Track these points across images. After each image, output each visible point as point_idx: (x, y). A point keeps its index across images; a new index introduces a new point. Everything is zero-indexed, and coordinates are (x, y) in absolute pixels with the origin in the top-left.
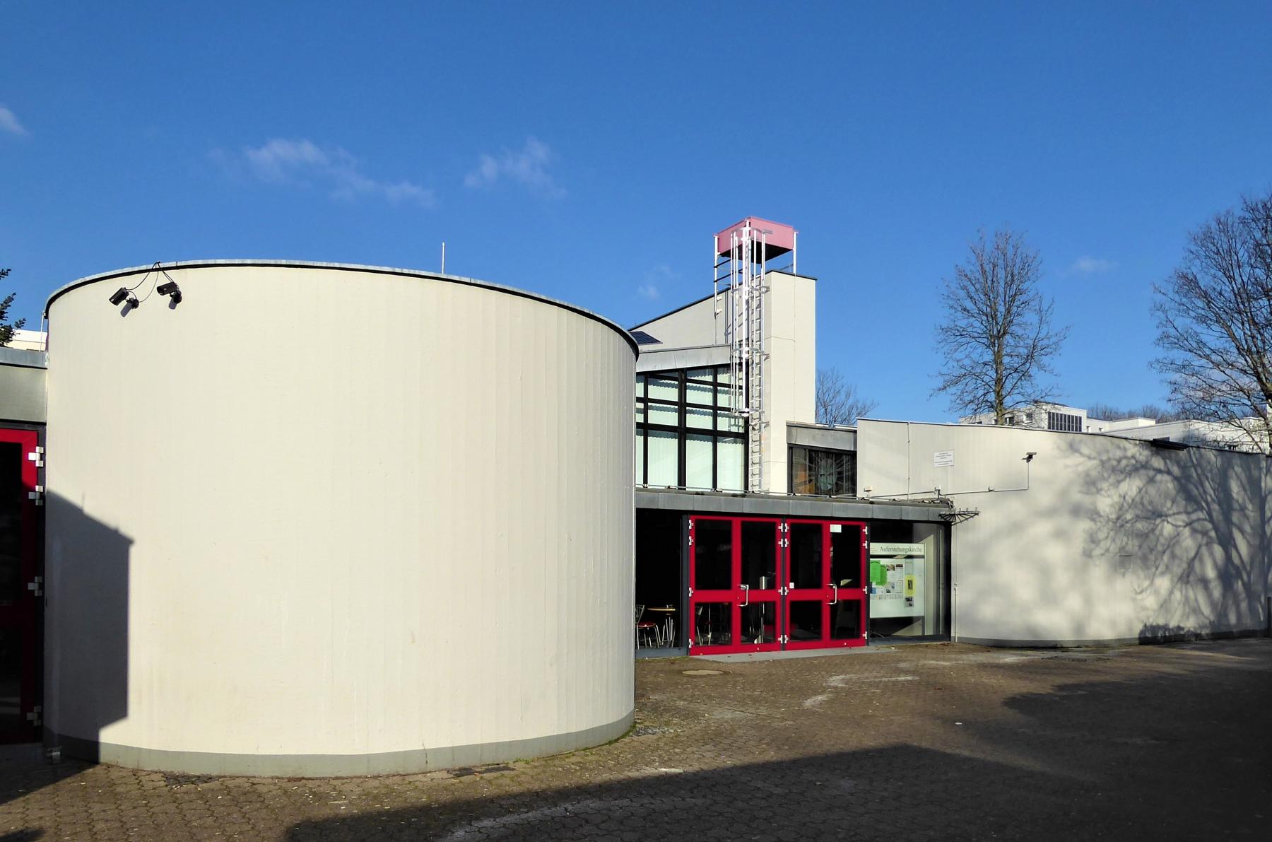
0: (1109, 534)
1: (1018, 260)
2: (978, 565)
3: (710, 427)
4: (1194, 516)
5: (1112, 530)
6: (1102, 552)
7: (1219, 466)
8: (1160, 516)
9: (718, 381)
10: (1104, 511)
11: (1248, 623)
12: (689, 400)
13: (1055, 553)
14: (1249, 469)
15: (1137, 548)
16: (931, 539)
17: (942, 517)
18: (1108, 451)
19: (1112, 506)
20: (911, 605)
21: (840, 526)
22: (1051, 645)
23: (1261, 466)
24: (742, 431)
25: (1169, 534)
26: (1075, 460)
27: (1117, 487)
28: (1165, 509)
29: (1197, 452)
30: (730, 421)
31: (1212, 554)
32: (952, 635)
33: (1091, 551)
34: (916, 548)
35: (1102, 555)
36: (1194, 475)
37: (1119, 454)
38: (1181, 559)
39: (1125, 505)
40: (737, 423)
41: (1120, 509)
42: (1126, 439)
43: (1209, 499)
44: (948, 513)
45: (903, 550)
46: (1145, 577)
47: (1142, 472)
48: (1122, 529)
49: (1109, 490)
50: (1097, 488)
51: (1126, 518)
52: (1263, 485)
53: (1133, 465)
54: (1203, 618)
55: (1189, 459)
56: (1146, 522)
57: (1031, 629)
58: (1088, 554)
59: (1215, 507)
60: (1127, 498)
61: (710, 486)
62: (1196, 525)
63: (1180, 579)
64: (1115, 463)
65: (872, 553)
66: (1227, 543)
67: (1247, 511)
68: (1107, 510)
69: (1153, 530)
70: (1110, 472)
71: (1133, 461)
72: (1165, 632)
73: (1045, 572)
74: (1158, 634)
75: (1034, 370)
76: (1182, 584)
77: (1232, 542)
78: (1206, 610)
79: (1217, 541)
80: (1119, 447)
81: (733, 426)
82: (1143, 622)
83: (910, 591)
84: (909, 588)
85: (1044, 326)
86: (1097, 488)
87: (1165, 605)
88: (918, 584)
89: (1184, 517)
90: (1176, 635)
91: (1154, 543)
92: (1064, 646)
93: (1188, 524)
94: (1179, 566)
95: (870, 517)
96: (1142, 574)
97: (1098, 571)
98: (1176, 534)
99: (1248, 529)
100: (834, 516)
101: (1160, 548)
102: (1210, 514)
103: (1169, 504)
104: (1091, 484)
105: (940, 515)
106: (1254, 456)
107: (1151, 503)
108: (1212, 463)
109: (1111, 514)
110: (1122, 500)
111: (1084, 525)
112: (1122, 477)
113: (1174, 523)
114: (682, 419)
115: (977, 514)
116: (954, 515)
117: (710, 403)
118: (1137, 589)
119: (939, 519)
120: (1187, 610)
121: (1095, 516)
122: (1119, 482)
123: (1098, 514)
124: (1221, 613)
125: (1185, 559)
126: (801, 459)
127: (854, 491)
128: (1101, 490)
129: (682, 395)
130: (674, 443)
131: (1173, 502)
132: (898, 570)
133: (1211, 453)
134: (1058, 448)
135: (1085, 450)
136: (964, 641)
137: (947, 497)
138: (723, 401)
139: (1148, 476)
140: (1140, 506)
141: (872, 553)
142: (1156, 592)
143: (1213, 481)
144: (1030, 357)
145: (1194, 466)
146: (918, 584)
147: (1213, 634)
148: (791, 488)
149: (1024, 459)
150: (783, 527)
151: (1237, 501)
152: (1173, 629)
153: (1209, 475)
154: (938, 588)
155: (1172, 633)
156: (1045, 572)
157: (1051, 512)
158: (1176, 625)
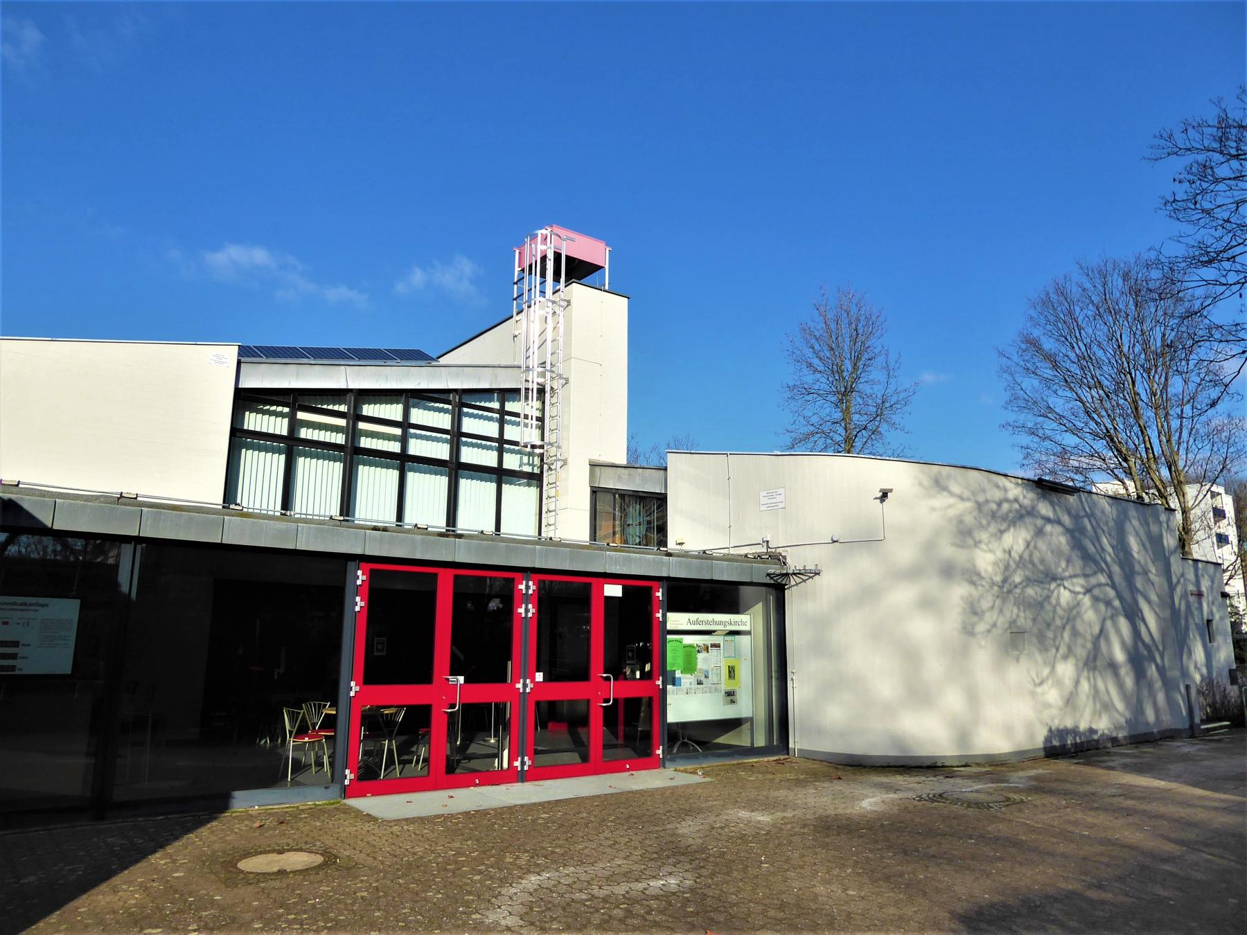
0: (994, 602)
1: (862, 318)
2: (820, 648)
3: (494, 464)
4: (1093, 581)
5: (998, 597)
6: (987, 627)
7: (1115, 517)
8: (1054, 579)
9: (506, 409)
10: (986, 571)
11: (1168, 721)
12: (465, 429)
13: (923, 629)
14: (1148, 524)
15: (1030, 623)
16: (759, 607)
17: (771, 578)
18: (984, 491)
19: (995, 564)
20: (733, 702)
21: (621, 586)
22: (928, 763)
23: (1161, 519)
24: (537, 471)
25: (1068, 604)
26: (942, 501)
27: (1000, 539)
28: (1060, 570)
29: (1089, 499)
30: (521, 458)
31: (1118, 631)
32: (791, 745)
33: (973, 625)
34: (742, 621)
35: (989, 631)
36: (1089, 527)
37: (998, 495)
38: (1084, 638)
39: (1011, 563)
40: (531, 462)
41: (1007, 567)
42: (1006, 476)
43: (1108, 559)
44: (778, 572)
45: (720, 623)
46: (1045, 663)
47: (1028, 520)
48: (1011, 597)
49: (990, 542)
50: (974, 540)
51: (1014, 581)
52: (1165, 543)
53: (1017, 511)
54: (1118, 716)
55: (1080, 507)
56: (1038, 586)
57: (897, 741)
58: (968, 631)
59: (1116, 569)
60: (1013, 554)
61: (393, 518)
62: (1096, 592)
63: (1086, 664)
64: (994, 506)
65: (670, 627)
66: (1133, 615)
67: (1150, 575)
68: (990, 569)
69: (1048, 598)
70: (989, 519)
71: (1017, 506)
72: (1075, 738)
73: (910, 656)
74: (1066, 741)
75: (884, 428)
76: (1089, 671)
77: (1140, 615)
78: (1120, 705)
79: (1123, 613)
80: (997, 486)
81: (525, 465)
82: (1047, 724)
83: (732, 681)
84: (730, 676)
85: (892, 380)
86: (974, 540)
87: (1070, 701)
88: (744, 672)
89: (1081, 581)
90: (1088, 742)
91: (1051, 616)
92: (946, 764)
93: (1088, 591)
94: (1084, 646)
95: (664, 574)
96: (1039, 658)
97: (983, 656)
98: (1075, 603)
99: (1154, 598)
100: (608, 571)
101: (1058, 622)
102: (1110, 577)
103: (1063, 564)
104: (964, 534)
105: (768, 575)
106: (1150, 507)
107: (1042, 561)
108: (1106, 512)
109: (995, 576)
110: (1007, 556)
111: (959, 592)
112: (1003, 527)
113: (1071, 588)
114: (456, 452)
115: (819, 574)
116: (787, 575)
117: (496, 435)
118: (1036, 679)
119: (768, 580)
120: (1098, 706)
121: (975, 578)
122: (1002, 532)
123: (979, 575)
124: (1137, 708)
125: (1089, 637)
126: (605, 505)
127: (663, 542)
128: (980, 542)
129: (457, 422)
130: (443, 481)
131: (1068, 561)
132: (713, 651)
133: (1104, 500)
134: (920, 484)
135: (955, 488)
136: (807, 755)
137: (778, 550)
138: (511, 433)
139: (1035, 525)
140: (1030, 566)
141: (670, 627)
142: (1059, 683)
143: (1110, 535)
144: (879, 415)
145: (1087, 515)
146: (744, 672)
147: (1131, 737)
148: (593, 535)
149: (876, 498)
150: (527, 587)
151: (1139, 563)
152: (1084, 734)
153: (1105, 528)
154: (770, 677)
155: (1084, 739)
156: (910, 656)
157: (913, 573)
158: (1087, 726)
